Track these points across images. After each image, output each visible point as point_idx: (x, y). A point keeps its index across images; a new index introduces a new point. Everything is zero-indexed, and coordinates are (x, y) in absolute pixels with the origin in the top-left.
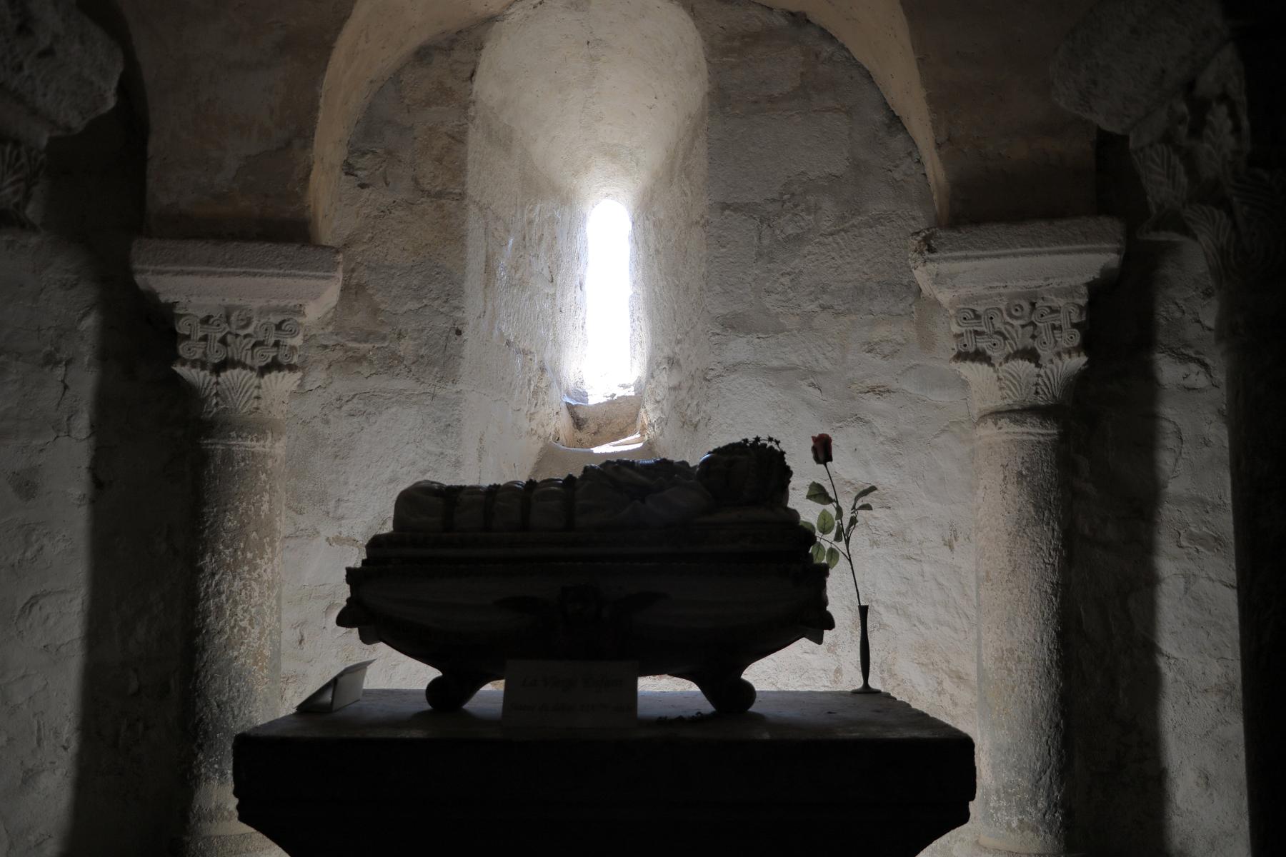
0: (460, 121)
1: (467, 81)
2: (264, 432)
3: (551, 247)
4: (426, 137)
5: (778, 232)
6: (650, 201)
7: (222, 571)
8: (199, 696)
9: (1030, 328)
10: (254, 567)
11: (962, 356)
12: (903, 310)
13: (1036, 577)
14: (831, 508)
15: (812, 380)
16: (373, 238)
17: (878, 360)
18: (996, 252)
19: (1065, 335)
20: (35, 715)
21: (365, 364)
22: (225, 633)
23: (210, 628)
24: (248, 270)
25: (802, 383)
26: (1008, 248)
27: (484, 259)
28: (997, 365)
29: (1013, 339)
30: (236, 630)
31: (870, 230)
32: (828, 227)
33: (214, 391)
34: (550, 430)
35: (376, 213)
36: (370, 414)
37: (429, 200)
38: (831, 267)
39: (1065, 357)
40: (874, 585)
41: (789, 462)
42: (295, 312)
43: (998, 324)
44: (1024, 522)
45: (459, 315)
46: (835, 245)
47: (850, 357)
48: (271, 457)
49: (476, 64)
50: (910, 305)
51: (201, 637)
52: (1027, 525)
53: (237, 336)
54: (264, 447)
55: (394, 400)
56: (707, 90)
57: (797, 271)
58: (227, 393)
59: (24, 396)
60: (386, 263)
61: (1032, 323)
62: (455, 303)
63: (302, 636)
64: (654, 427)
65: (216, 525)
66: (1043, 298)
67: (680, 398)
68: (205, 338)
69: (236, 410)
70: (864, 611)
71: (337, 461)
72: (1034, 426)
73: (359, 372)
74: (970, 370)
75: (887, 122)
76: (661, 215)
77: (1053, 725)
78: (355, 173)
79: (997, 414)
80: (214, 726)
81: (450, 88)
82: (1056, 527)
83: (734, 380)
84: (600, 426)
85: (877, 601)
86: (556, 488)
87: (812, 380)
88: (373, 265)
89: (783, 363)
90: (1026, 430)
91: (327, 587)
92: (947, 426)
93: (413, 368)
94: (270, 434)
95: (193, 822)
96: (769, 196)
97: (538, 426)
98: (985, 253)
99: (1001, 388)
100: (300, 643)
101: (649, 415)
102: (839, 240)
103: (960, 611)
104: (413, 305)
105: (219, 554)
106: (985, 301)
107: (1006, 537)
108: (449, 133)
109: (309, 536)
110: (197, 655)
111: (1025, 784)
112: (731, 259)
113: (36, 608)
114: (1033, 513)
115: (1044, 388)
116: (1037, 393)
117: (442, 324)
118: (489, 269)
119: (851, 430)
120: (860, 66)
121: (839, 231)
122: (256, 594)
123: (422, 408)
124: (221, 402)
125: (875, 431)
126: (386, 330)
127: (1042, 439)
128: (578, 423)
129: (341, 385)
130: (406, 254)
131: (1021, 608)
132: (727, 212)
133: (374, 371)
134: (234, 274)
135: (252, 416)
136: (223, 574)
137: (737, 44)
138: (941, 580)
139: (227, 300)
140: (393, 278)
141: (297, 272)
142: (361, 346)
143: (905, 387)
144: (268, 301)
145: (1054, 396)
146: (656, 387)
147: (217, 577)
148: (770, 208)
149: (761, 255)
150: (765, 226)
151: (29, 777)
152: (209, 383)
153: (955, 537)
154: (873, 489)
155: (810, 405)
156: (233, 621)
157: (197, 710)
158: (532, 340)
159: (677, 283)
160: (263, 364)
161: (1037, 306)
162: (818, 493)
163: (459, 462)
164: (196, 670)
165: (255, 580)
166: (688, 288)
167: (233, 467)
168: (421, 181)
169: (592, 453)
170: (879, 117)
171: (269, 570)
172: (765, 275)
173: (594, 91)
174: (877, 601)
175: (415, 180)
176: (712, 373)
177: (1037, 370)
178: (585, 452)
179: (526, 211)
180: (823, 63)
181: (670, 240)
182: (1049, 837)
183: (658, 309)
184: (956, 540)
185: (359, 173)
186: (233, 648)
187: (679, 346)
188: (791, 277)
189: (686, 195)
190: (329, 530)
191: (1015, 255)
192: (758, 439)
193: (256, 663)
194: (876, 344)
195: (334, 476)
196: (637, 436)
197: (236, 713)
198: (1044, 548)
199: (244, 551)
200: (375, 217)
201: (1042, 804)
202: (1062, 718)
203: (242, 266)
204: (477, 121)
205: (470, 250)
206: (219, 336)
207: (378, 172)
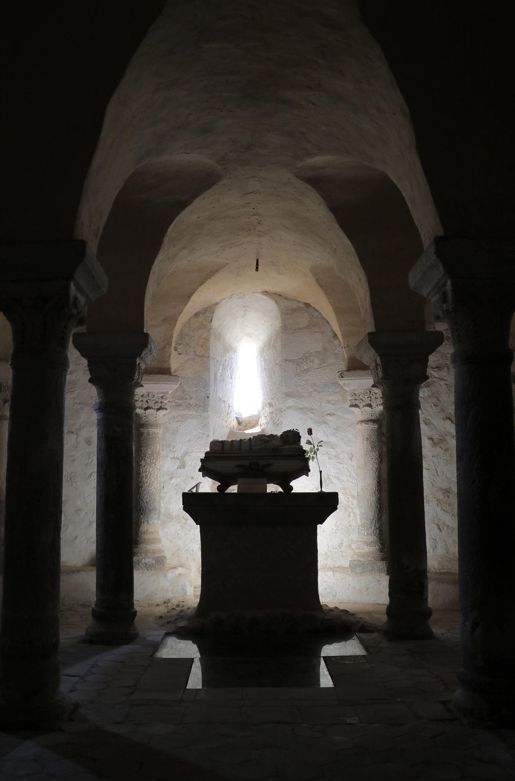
0: (208, 334)
1: (210, 322)
2: (158, 427)
3: (231, 367)
4: (198, 339)
5: (302, 368)
6: (263, 352)
7: (147, 465)
8: (141, 500)
9: (370, 398)
10: (155, 465)
11: (351, 406)
12: (338, 391)
13: (371, 466)
14: (312, 446)
15: (312, 411)
16: (183, 369)
17: (331, 406)
18: (359, 378)
19: (379, 400)
21: (181, 407)
22: (148, 482)
23: (144, 481)
24: (155, 382)
25: (309, 412)
26: (362, 377)
27: (214, 374)
28: (361, 408)
29: (365, 401)
30: (151, 482)
31: (328, 368)
32: (316, 367)
33: (144, 415)
34: (232, 426)
35: (184, 362)
36: (183, 421)
37: (199, 358)
38: (317, 378)
39: (379, 406)
40: (329, 471)
41: (301, 434)
42: (166, 393)
43: (361, 397)
44: (368, 451)
45: (208, 392)
46: (318, 372)
47: (323, 405)
48: (159, 434)
49: (212, 317)
50: (340, 390)
51: (141, 484)
52: (369, 452)
53: (151, 400)
54: (157, 431)
55: (190, 417)
56: (281, 325)
57: (307, 379)
58: (148, 416)
59: (88, 416)
60: (187, 377)
61: (370, 397)
62: (207, 388)
63: (164, 486)
64: (264, 424)
65: (145, 453)
66: (373, 390)
67: (273, 416)
68: (142, 401)
69: (150, 420)
70: (321, 472)
71: (173, 435)
72: (371, 425)
73: (179, 409)
74: (353, 409)
75: (333, 336)
76: (266, 357)
77: (376, 507)
78: (177, 350)
79: (362, 422)
80: (145, 508)
81: (205, 324)
82: (377, 452)
83: (289, 411)
84: (246, 424)
85: (330, 475)
86: (267, 438)
87: (312, 411)
88: (183, 377)
89: (303, 406)
90: (369, 426)
91: (170, 472)
92: (350, 425)
93: (195, 408)
94: (159, 427)
95: (140, 534)
96: (299, 357)
97: (228, 424)
98: (356, 378)
99: (363, 415)
100: (163, 488)
101: (263, 421)
102: (319, 371)
103: (354, 478)
104: (195, 389)
105: (146, 461)
106: (357, 391)
107: (363, 456)
108: (205, 338)
109: (165, 457)
110: (140, 489)
111: (369, 523)
112: (288, 376)
113: (92, 476)
114: (371, 449)
115: (374, 414)
116: (372, 416)
117: (203, 395)
118: (215, 378)
119: (323, 426)
120: (325, 319)
121: (319, 368)
122: (156, 472)
123: (198, 420)
124: (146, 418)
125: (330, 426)
126: (187, 397)
127: (373, 428)
128: (239, 423)
129: (174, 413)
130: (192, 374)
131: (367, 475)
132: (287, 362)
133: (183, 409)
134: (151, 383)
135: (154, 422)
136: (147, 466)
137: (289, 312)
138: (349, 469)
139: (149, 390)
140: (189, 381)
141: (168, 383)
142: (180, 401)
143: (338, 413)
144: (159, 390)
145: (377, 417)
146: (265, 412)
147: (146, 467)
148: (299, 361)
149: (297, 375)
150: (298, 366)
152: (143, 413)
153: (353, 457)
154: (322, 441)
155: (311, 418)
157: (140, 504)
158: (226, 397)
159: (272, 380)
160: (158, 408)
161: (371, 392)
162: (309, 442)
163: (208, 435)
165: (156, 468)
166: (275, 383)
167: (150, 436)
168: (197, 352)
169: (245, 433)
170: (331, 334)
171: (159, 466)
172: (298, 381)
173: (245, 319)
174: (330, 475)
175: (195, 352)
176: (283, 409)
177: (372, 410)
178: (243, 432)
179: (224, 357)
180: (315, 318)
181: (269, 366)
182: (375, 537)
183: (265, 387)
184: (353, 458)
185: (178, 350)
187: (273, 400)
188: (306, 381)
189: (274, 354)
190: (171, 455)
191: (364, 379)
192: (293, 429)
193: (156, 491)
194: (330, 401)
195: (172, 440)
196: (259, 427)
197: (151, 505)
198: (374, 458)
200: (183, 363)
201: (373, 528)
202: (379, 505)
203: (154, 381)
204: (212, 334)
205: (211, 373)
206: (146, 400)
207: (184, 350)
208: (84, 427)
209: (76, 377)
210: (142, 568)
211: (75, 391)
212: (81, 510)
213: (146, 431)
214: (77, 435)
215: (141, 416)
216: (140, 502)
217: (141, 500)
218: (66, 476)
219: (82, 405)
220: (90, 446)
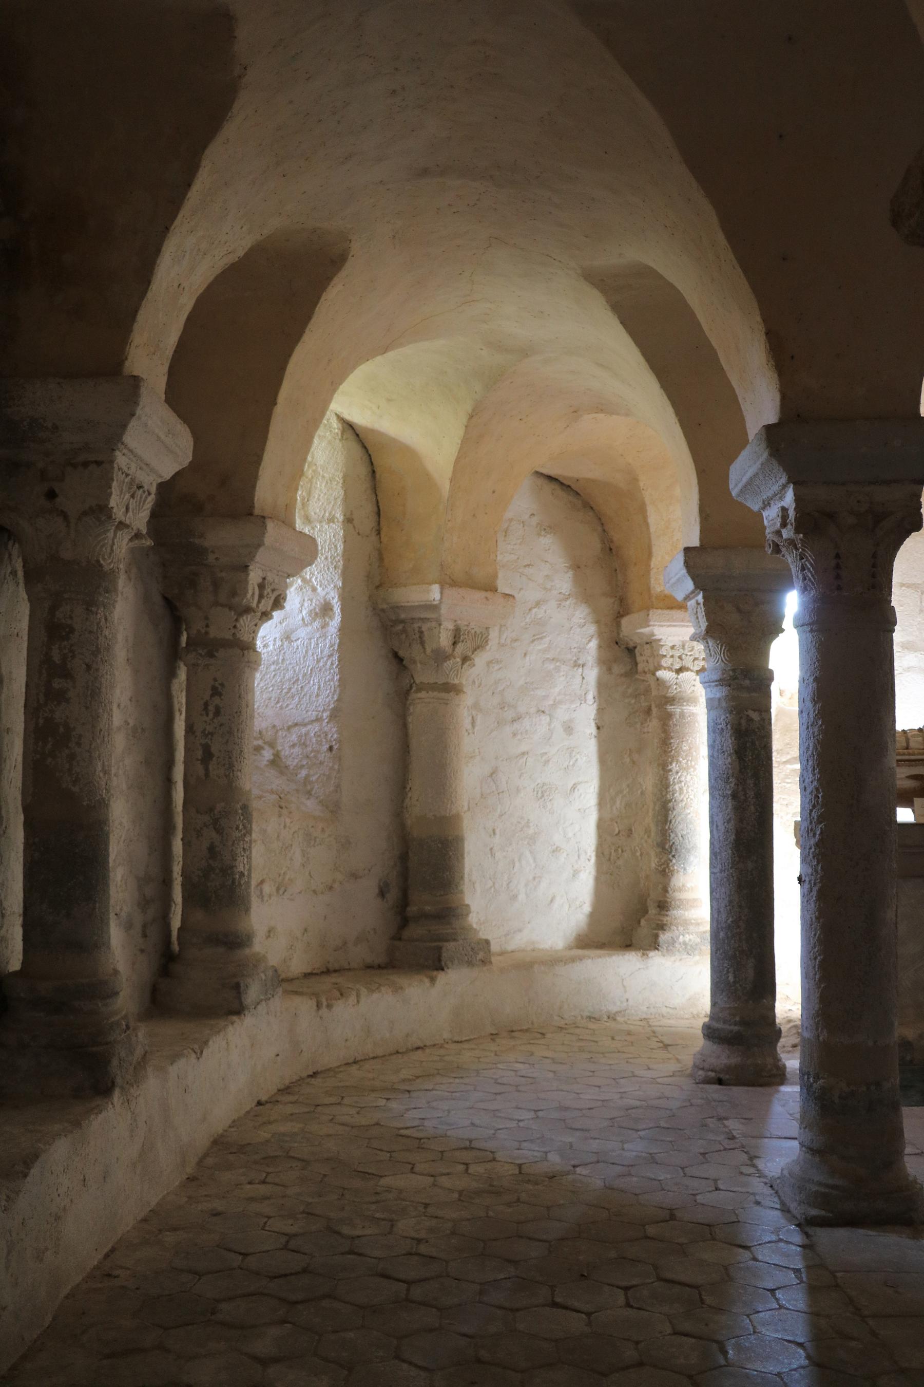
10: (695, 769)
20: (577, 843)
30: (689, 800)
33: (675, 682)
53: (687, 655)
58: (682, 683)
59: (567, 683)
68: (672, 656)
95: (671, 892)
113: (576, 790)
132: (904, 588)
147: (679, 774)
151: (576, 873)
156: (687, 796)
164: (669, 819)
186: (688, 809)
199: (691, 761)
208: (560, 702)
209: (545, 612)
210: (679, 951)
211: (545, 637)
212: (560, 850)
213: (678, 710)
214: (550, 715)
215: (668, 684)
216: (670, 836)
217: (672, 832)
218: (536, 790)
219: (557, 662)
220: (571, 737)
